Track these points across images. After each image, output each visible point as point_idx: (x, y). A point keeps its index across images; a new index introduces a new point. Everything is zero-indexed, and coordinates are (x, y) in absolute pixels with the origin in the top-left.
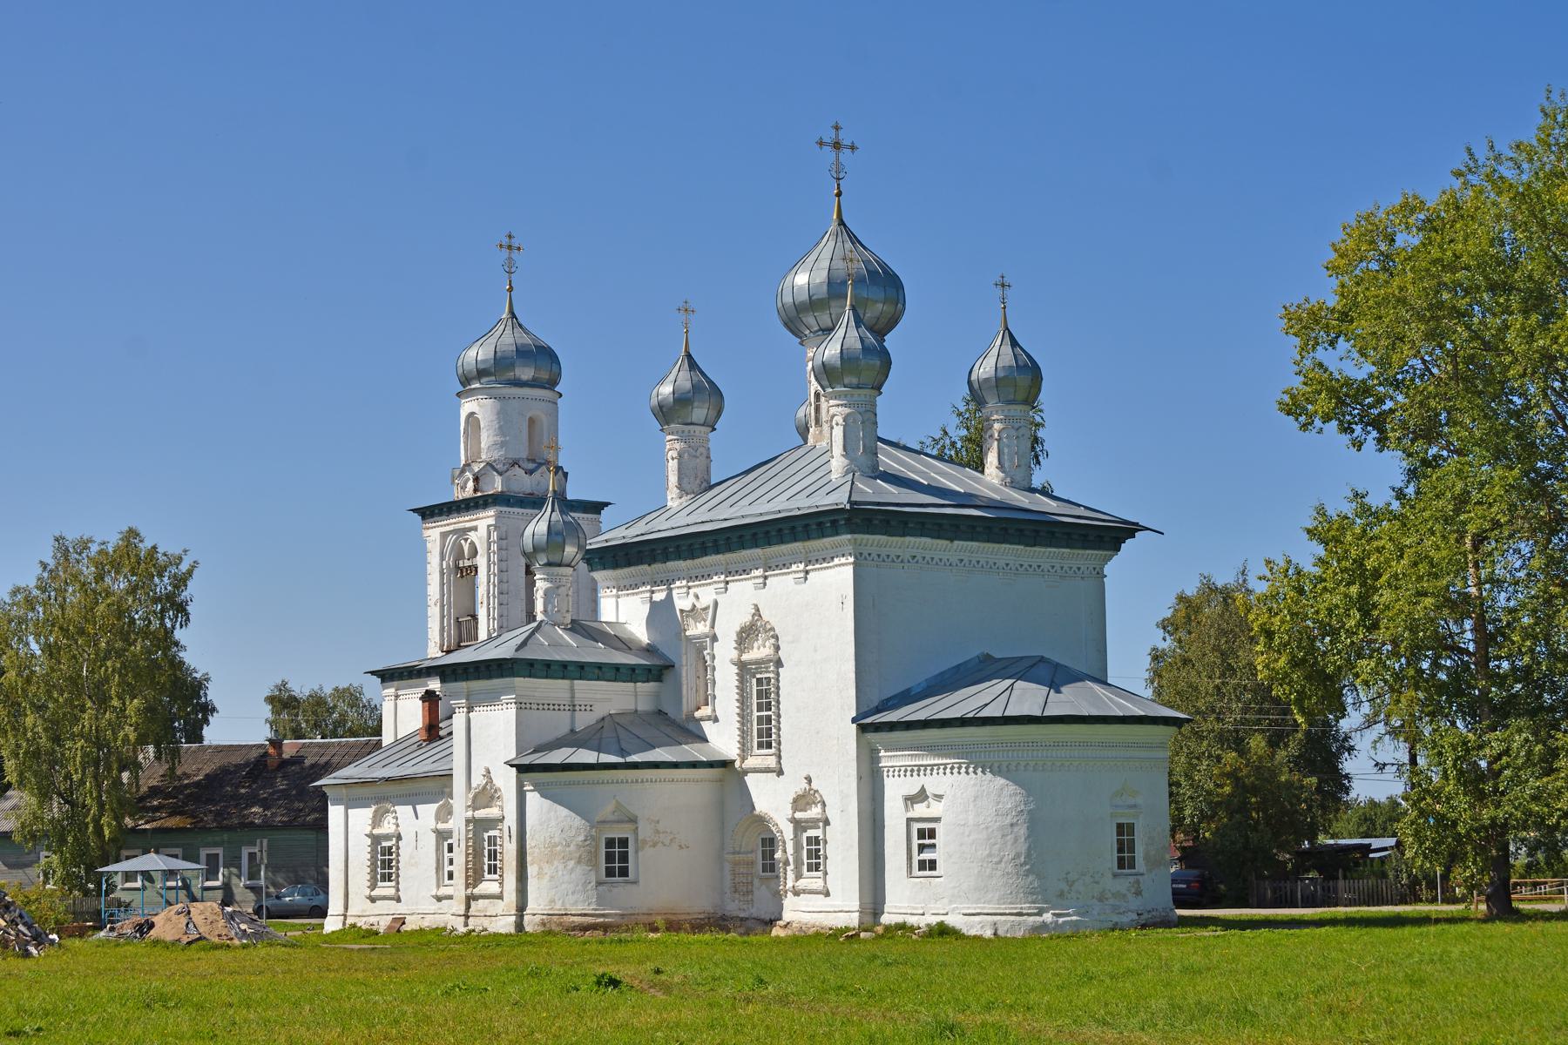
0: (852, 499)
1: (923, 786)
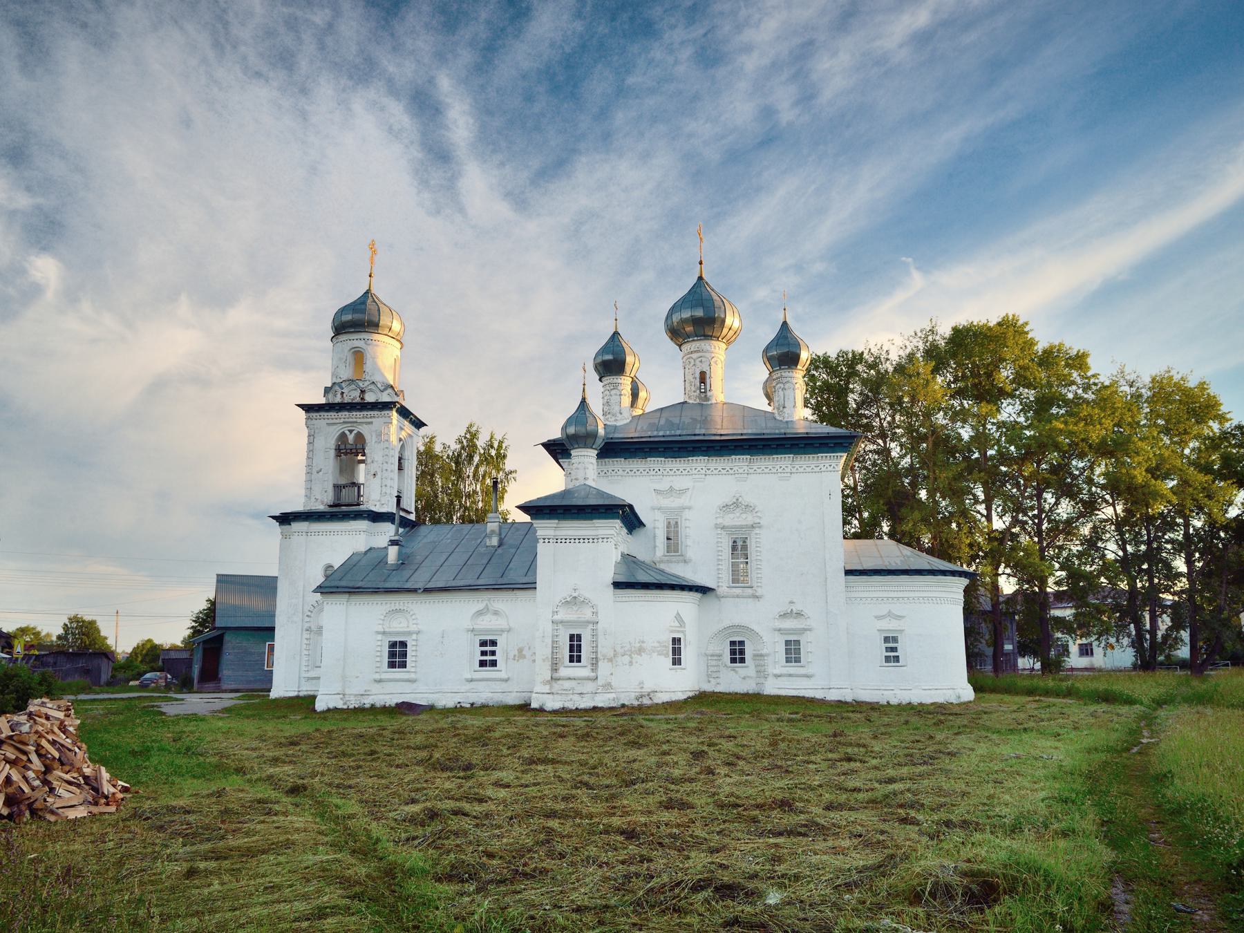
0: (227, 638)
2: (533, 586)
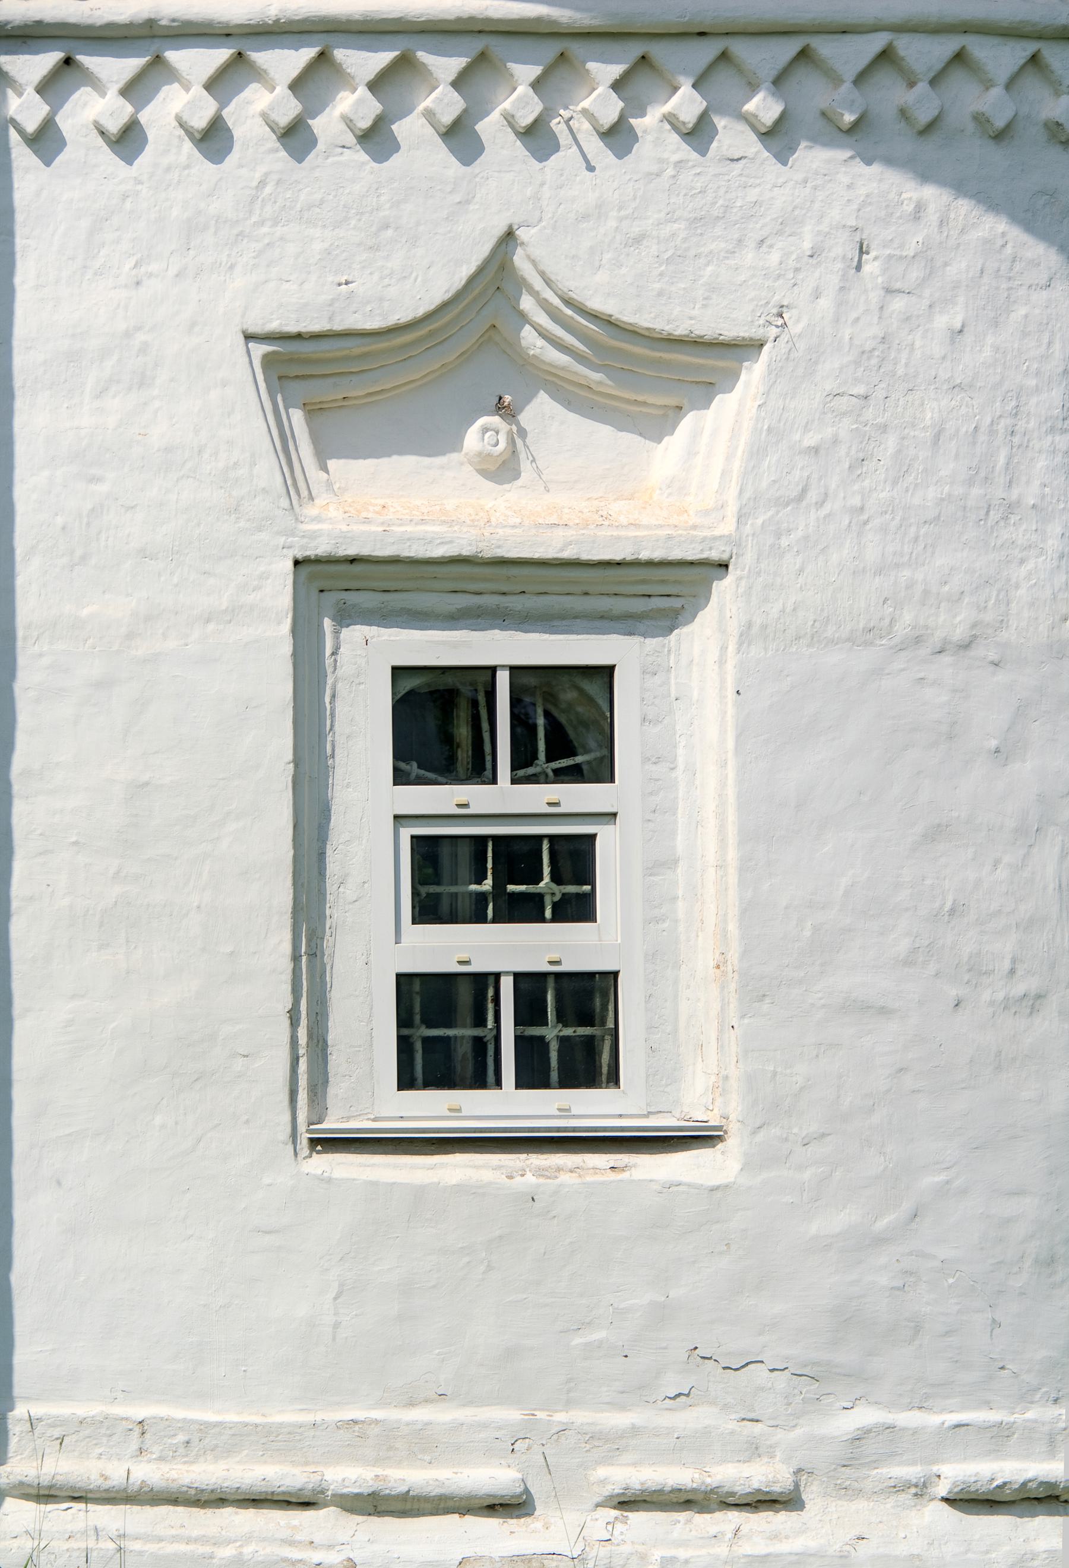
1: (615, 665)
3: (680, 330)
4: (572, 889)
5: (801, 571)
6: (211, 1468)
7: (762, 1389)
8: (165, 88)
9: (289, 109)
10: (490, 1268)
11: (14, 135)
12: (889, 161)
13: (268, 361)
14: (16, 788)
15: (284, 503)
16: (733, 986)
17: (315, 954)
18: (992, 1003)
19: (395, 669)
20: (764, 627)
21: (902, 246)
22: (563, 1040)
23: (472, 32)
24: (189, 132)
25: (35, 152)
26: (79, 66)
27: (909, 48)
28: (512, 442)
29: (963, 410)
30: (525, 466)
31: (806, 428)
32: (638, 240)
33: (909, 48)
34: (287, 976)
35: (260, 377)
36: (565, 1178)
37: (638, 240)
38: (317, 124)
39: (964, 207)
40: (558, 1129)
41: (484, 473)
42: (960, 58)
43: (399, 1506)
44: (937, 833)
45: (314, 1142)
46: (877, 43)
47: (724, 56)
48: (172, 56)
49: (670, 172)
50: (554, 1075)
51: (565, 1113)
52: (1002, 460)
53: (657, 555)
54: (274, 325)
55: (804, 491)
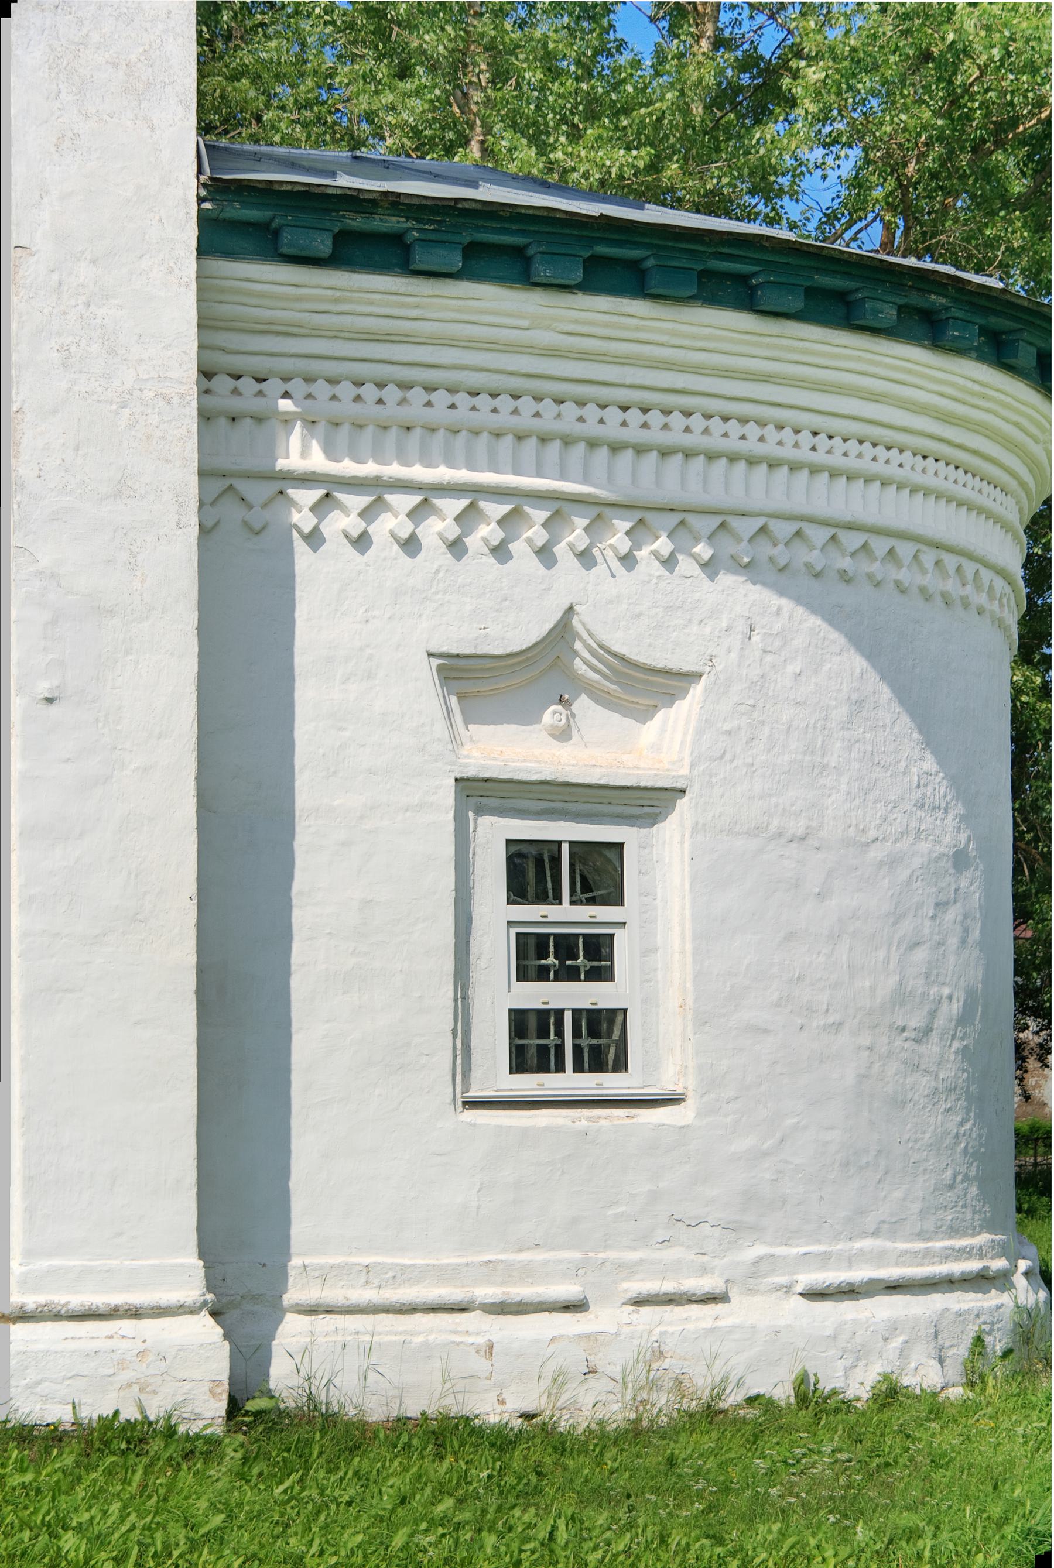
2: (237, 211)
3: (660, 665)
4: (595, 963)
5: (723, 795)
6: (408, 1291)
7: (707, 1237)
8: (383, 515)
9: (454, 532)
10: (563, 1173)
11: (295, 534)
12: (764, 584)
13: (440, 668)
14: (294, 902)
15: (450, 747)
16: (690, 1017)
17: (465, 997)
18: (818, 1027)
19: (508, 841)
20: (704, 825)
21: (771, 628)
22: (591, 1046)
23: (552, 498)
24: (397, 540)
25: (308, 544)
26: (335, 499)
27: (775, 526)
28: (568, 720)
29: (801, 716)
30: (575, 733)
31: (725, 721)
32: (638, 616)
33: (775, 526)
34: (451, 1010)
35: (436, 677)
36: (603, 1122)
37: (638, 616)
38: (468, 541)
39: (800, 611)
40: (598, 1095)
41: (553, 736)
42: (798, 534)
43: (515, 1309)
44: (790, 937)
45: (465, 1103)
46: (760, 522)
47: (682, 523)
48: (389, 498)
49: (654, 581)
50: (586, 1066)
51: (600, 1086)
52: (820, 742)
53: (649, 784)
54: (444, 649)
55: (724, 753)
